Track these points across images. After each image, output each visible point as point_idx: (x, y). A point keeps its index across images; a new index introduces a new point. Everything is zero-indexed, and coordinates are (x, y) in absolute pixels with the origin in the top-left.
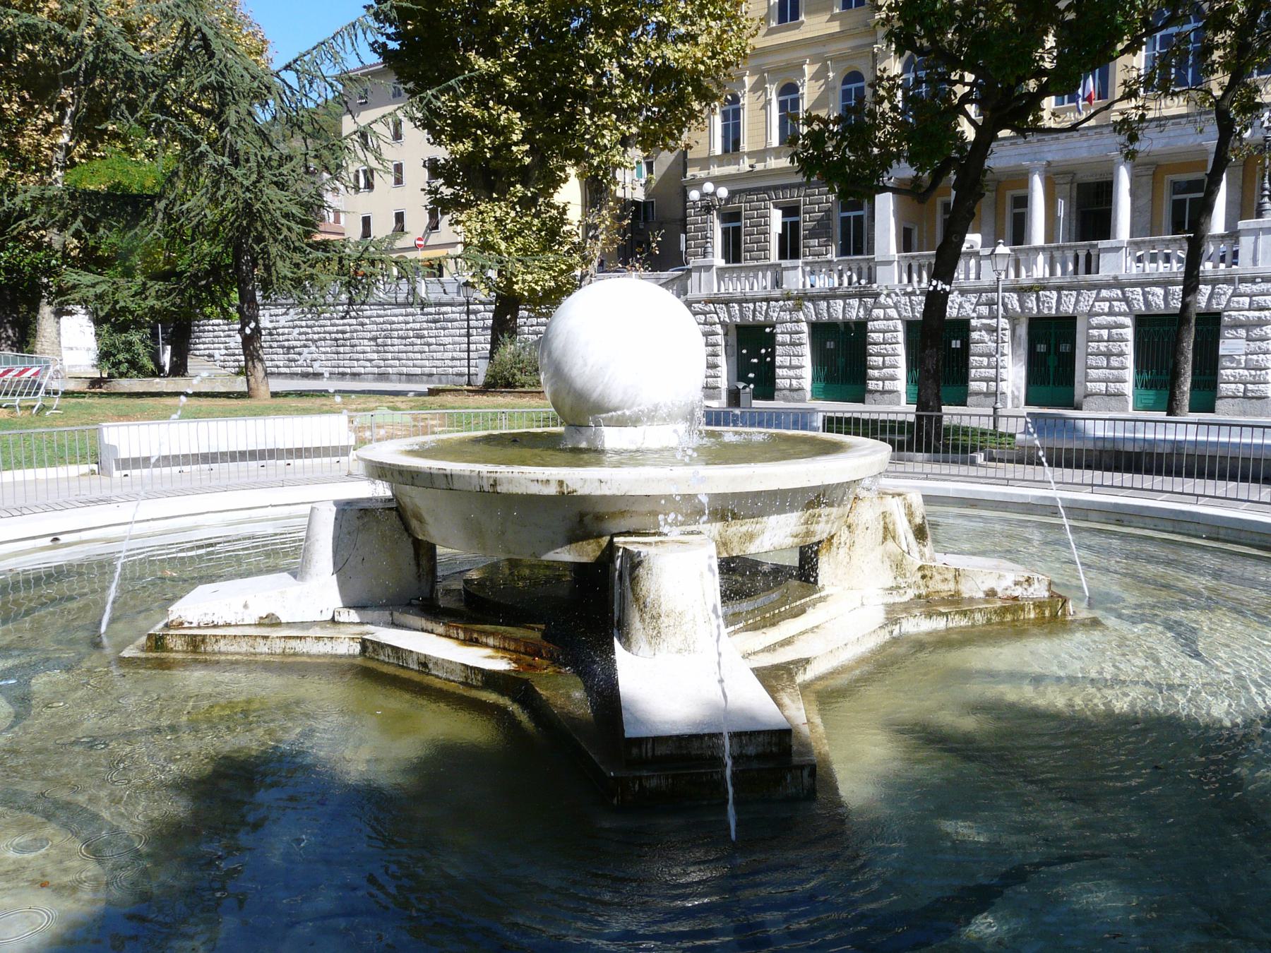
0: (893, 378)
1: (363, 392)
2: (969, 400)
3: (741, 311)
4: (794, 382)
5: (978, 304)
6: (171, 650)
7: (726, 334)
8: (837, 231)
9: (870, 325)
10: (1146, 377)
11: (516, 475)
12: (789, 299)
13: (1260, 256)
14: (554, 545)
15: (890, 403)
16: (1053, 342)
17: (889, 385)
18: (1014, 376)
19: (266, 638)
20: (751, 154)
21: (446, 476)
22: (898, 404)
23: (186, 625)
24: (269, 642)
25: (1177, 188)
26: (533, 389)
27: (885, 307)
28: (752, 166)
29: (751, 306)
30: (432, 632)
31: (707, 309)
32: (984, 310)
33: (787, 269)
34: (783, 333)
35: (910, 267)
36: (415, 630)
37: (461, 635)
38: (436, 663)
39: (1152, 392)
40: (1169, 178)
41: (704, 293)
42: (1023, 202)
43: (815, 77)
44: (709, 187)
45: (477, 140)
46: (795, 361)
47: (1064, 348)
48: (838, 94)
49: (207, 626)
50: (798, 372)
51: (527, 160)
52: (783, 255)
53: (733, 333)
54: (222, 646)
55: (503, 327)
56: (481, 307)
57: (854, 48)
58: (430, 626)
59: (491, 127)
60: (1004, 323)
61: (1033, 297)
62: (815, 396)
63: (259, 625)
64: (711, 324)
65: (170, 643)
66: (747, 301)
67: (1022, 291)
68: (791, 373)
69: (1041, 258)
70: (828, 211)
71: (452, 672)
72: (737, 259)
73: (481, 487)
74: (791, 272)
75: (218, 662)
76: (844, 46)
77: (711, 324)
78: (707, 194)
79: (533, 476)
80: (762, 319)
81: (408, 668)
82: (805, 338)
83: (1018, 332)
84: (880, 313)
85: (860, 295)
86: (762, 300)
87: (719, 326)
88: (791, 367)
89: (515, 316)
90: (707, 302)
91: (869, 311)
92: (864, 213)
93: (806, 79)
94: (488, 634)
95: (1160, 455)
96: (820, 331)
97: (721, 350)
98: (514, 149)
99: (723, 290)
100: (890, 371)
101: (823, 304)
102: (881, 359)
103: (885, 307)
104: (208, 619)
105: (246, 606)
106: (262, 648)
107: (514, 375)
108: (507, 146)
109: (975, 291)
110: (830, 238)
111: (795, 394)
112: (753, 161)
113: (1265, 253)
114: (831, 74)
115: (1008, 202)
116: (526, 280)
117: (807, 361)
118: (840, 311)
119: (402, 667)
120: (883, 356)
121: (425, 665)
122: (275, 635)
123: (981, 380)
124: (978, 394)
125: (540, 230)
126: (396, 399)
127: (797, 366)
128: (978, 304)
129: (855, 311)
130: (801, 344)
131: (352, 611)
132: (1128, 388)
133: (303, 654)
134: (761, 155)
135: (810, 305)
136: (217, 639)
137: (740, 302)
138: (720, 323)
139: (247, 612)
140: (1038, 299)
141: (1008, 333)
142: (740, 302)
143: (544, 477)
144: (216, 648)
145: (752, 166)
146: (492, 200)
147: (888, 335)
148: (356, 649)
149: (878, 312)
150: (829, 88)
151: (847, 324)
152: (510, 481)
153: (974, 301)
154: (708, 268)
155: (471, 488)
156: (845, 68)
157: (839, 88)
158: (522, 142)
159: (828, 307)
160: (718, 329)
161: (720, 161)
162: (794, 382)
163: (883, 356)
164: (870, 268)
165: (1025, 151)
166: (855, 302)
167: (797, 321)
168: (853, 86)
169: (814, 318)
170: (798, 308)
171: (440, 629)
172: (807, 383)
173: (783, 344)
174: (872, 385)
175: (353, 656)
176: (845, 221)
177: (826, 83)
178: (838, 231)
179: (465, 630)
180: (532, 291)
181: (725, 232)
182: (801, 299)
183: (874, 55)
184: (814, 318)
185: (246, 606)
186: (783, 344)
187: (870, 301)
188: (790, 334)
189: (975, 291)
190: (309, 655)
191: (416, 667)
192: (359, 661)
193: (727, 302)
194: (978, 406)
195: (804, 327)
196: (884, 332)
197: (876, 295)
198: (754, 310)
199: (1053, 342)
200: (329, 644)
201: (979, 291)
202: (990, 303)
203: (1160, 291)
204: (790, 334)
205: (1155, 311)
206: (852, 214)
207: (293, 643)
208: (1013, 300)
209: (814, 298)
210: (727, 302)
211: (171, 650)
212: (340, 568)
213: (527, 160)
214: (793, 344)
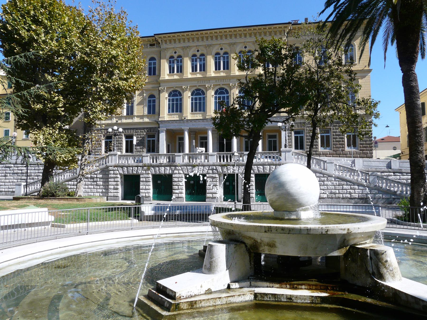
0: (181, 193)
1: (7, 200)
2: (207, 200)
3: (127, 170)
4: (147, 194)
5: (208, 170)
6: (183, 309)
7: (121, 178)
8: (146, 144)
9: (174, 176)
10: (258, 192)
11: (335, 228)
12: (145, 166)
13: (287, 158)
14: (333, 250)
15: (181, 201)
16: (231, 182)
17: (180, 195)
18: (220, 192)
19: (220, 298)
20: (138, 116)
21: (308, 229)
22: (183, 201)
23: (182, 298)
24: (221, 300)
25: (270, 137)
26: (63, 197)
27: (178, 170)
28: (117, 121)
29: (131, 168)
30: (273, 287)
31: (115, 169)
32: (210, 171)
33: (145, 156)
34: (143, 178)
35: (223, 157)
36: (264, 287)
37: (288, 286)
38: (297, 297)
39: (189, 196)
40: (267, 134)
41: (113, 163)
42: (206, 138)
43: (139, 95)
44: (115, 128)
45: (45, 105)
46: (147, 187)
47: (228, 183)
48: (147, 101)
49: (189, 297)
50: (148, 191)
51: (63, 113)
52: (127, 151)
53: (123, 177)
54: (203, 304)
55: (47, 175)
56: (13, 165)
57: (152, 87)
58: (271, 285)
59: (51, 101)
60: (217, 176)
61: (226, 168)
62: (154, 199)
63: (205, 294)
64: (116, 174)
65: (182, 306)
66: (130, 167)
67: (222, 166)
68: (146, 191)
69: (203, 157)
70: (143, 138)
71: (305, 299)
72: (132, 151)
73: (322, 232)
74: (146, 158)
75: (204, 312)
76: (149, 87)
77: (116, 174)
78: (115, 130)
79: (341, 228)
80: (135, 173)
81: (281, 301)
82: (151, 179)
83: (221, 178)
84: (177, 172)
85: (170, 166)
86: (135, 166)
87: (119, 175)
88: (146, 189)
89: (53, 170)
90: (114, 167)
91: (173, 171)
92: (156, 139)
93: (136, 95)
94: (302, 285)
95: (150, 216)
96: (156, 177)
97: (119, 183)
98: (58, 109)
99: (120, 163)
100: (180, 190)
101: (157, 168)
102: (177, 187)
103: (178, 170)
104: (189, 294)
105: (201, 287)
106: (218, 302)
107: (55, 192)
108: (55, 108)
109: (208, 166)
110: (144, 146)
111: (147, 199)
112: (117, 120)
113: (288, 157)
114: (145, 95)
115: (177, 139)
116: (62, 156)
117: (151, 187)
118: (163, 171)
119: (278, 301)
120: (178, 186)
121: (290, 299)
122: (223, 296)
123: (210, 193)
124: (208, 198)
125: (66, 139)
126: (19, 202)
127: (147, 189)
128: (208, 170)
129: (168, 171)
130: (149, 182)
131: (237, 284)
132: (184, 195)
133: (233, 303)
134: (142, 117)
135: (153, 169)
136: (201, 301)
137: (127, 167)
138: (119, 174)
139: (202, 289)
140: (227, 168)
141: (218, 179)
142: (127, 167)
143: (344, 228)
144: (200, 305)
145: (117, 121)
146: (47, 127)
147: (180, 179)
148: (252, 297)
149: (175, 171)
150: (144, 99)
151: (165, 175)
152: (333, 230)
153: (207, 169)
154: (115, 155)
155: (318, 233)
156: (150, 93)
157: (147, 99)
158: (62, 107)
159: (159, 170)
160: (119, 176)
161: (126, 118)
162: (147, 194)
163: (178, 186)
164: (173, 158)
165: (207, 123)
166: (168, 168)
167: (148, 174)
168: (152, 99)
169: (154, 173)
170: (148, 169)
171: (278, 285)
172: (151, 195)
173: (143, 181)
174: (208, 195)
175: (251, 301)
176: (149, 141)
177: (143, 97)
178: (146, 144)
179: (290, 285)
180: (64, 160)
181: (127, 142)
182: (149, 166)
183: (159, 91)
184: (154, 173)
185: (201, 287)
186: (143, 181)
187: (173, 168)
188: (145, 178)
189: (208, 166)
190: (235, 303)
191: (286, 300)
192: (255, 302)
193: (122, 167)
194: (209, 202)
195: (151, 176)
196: (178, 178)
197: (176, 166)
198: (132, 170)
199: (231, 182)
200: (243, 297)
201: (209, 166)
202: (213, 170)
203: (262, 167)
204: (145, 178)
205: (261, 173)
206: (151, 139)
207: (230, 299)
208: (219, 169)
209: (154, 167)
210: (122, 167)
211: (183, 309)
212: (229, 267)
213: (63, 113)
214: (146, 181)
